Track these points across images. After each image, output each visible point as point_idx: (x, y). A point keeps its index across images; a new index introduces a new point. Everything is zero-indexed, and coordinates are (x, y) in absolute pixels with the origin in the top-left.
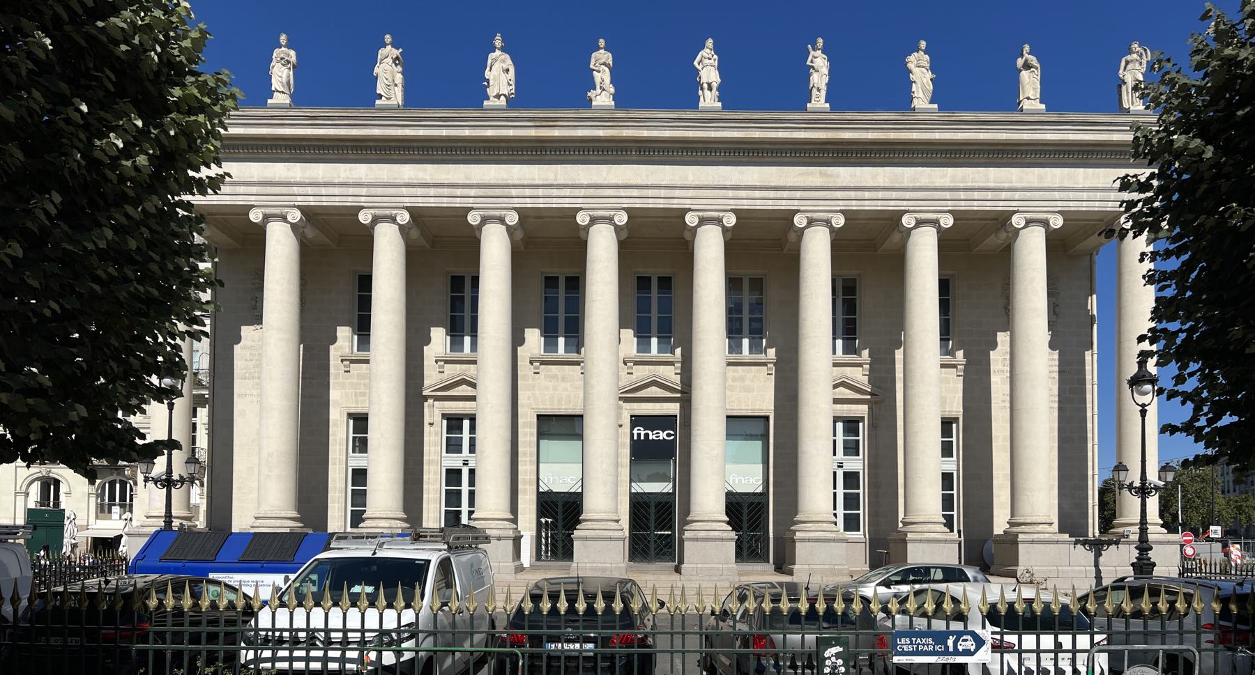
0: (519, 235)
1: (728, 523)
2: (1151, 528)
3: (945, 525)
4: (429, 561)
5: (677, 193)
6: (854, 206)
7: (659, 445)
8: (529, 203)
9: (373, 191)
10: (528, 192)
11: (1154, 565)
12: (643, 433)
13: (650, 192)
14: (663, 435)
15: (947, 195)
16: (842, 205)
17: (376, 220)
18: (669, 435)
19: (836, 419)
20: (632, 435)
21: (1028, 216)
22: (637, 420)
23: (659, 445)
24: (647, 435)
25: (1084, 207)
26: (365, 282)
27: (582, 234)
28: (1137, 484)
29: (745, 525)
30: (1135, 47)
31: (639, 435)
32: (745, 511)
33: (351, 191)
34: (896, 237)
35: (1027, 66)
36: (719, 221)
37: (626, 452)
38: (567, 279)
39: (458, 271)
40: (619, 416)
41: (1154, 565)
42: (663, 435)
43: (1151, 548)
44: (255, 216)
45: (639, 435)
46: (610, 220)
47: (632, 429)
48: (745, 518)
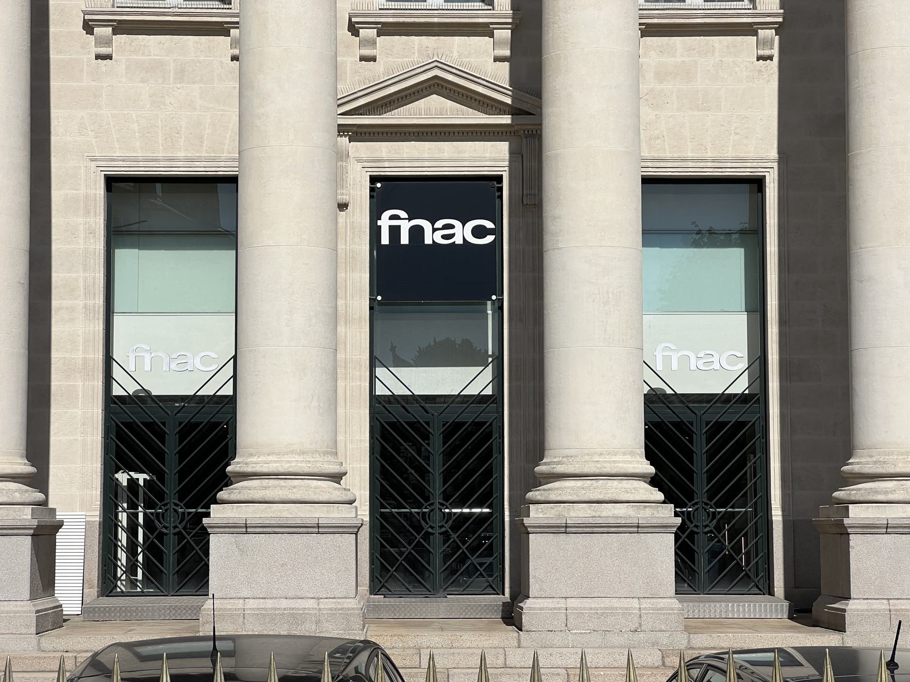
1: (654, 482)
20: (375, 232)
24: (417, 232)
31: (395, 231)
45: (395, 231)
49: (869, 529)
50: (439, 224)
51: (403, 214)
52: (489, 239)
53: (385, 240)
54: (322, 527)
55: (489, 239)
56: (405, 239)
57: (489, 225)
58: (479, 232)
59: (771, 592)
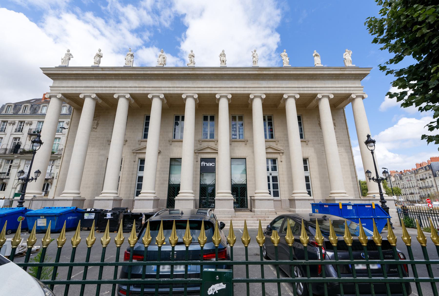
0: (198, 102)
2: (384, 195)
3: (308, 194)
4: (331, 276)
5: (213, 89)
6: (268, 92)
7: (207, 167)
8: (167, 92)
9: (119, 89)
10: (167, 89)
11: (388, 208)
12: (204, 164)
13: (205, 89)
14: (211, 164)
15: (297, 89)
16: (265, 92)
17: (153, 97)
18: (213, 164)
19: (267, 159)
20: (201, 164)
21: (323, 95)
22: (202, 160)
23: (207, 167)
24: (206, 164)
25: (339, 92)
26: (148, 118)
27: (217, 102)
28: (375, 178)
29: (239, 195)
30: (347, 50)
31: (203, 164)
32: (239, 190)
33: (113, 89)
34: (314, 102)
35: (316, 55)
36: (124, 97)
37: (199, 170)
38: (239, 117)
39: (178, 114)
40: (197, 158)
41: (388, 208)
42: (211, 164)
43: (386, 202)
44: (150, 96)
45: (203, 164)
46: (192, 97)
47: (201, 162)
48: (239, 192)
58: (213, 164)
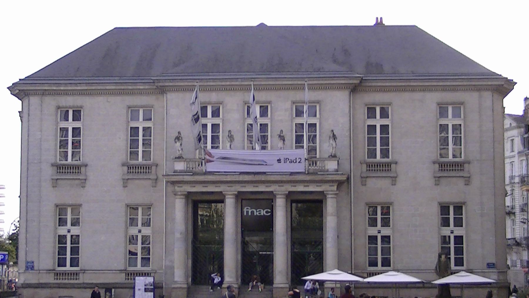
20: (242, 212)
24: (252, 212)
31: (247, 212)
45: (247, 212)
49: (228, 198)
50: (258, 210)
51: (249, 208)
52: (269, 214)
53: (245, 214)
54: (459, 288)
55: (269, 214)
56: (250, 214)
57: (269, 210)
58: (267, 212)
59: (460, 117)
